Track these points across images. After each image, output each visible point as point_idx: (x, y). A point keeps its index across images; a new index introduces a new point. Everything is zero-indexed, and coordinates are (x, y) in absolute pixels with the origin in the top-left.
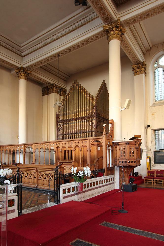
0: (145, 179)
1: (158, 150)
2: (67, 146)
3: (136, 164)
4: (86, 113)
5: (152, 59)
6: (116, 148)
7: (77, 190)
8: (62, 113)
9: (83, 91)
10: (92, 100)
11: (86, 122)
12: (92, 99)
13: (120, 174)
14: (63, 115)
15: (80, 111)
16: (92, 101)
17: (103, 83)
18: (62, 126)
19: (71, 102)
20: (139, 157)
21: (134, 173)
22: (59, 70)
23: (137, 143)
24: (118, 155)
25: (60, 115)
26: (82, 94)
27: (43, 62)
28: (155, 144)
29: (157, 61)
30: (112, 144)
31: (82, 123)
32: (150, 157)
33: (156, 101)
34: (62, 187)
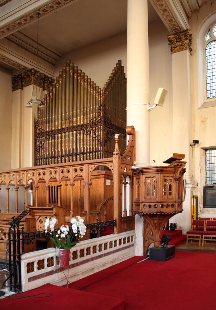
0: (188, 235)
1: (210, 183)
2: (47, 177)
3: (176, 209)
4: (87, 119)
5: (201, 26)
6: (139, 180)
7: (58, 263)
8: (44, 120)
9: (81, 79)
10: (97, 94)
11: (87, 135)
12: (98, 93)
13: (144, 229)
14: (46, 124)
15: (75, 114)
16: (97, 97)
17: (118, 65)
18: (43, 142)
19: (60, 99)
20: (180, 196)
21: (170, 225)
22: (38, 43)
23: (177, 169)
24: (141, 194)
25: (41, 124)
26: (79, 84)
27: (11, 27)
28: (206, 174)
29: (209, 31)
30: (130, 172)
31: (78, 136)
32: (197, 197)
33: (208, 98)
34: (26, 258)
